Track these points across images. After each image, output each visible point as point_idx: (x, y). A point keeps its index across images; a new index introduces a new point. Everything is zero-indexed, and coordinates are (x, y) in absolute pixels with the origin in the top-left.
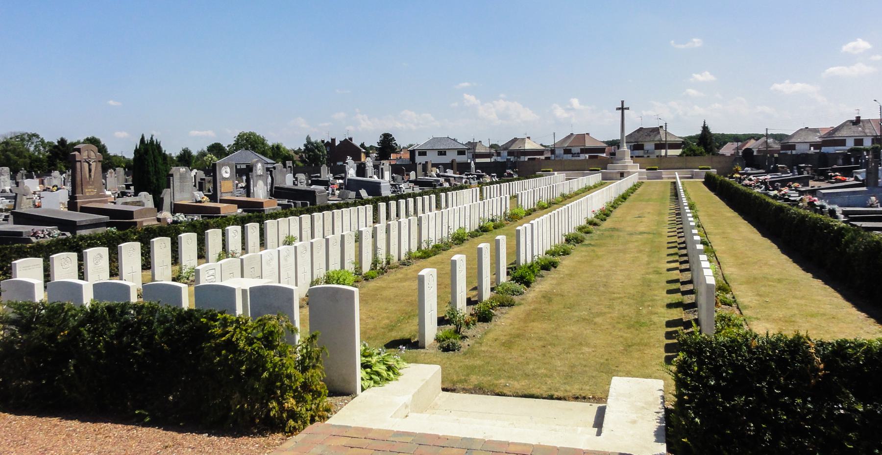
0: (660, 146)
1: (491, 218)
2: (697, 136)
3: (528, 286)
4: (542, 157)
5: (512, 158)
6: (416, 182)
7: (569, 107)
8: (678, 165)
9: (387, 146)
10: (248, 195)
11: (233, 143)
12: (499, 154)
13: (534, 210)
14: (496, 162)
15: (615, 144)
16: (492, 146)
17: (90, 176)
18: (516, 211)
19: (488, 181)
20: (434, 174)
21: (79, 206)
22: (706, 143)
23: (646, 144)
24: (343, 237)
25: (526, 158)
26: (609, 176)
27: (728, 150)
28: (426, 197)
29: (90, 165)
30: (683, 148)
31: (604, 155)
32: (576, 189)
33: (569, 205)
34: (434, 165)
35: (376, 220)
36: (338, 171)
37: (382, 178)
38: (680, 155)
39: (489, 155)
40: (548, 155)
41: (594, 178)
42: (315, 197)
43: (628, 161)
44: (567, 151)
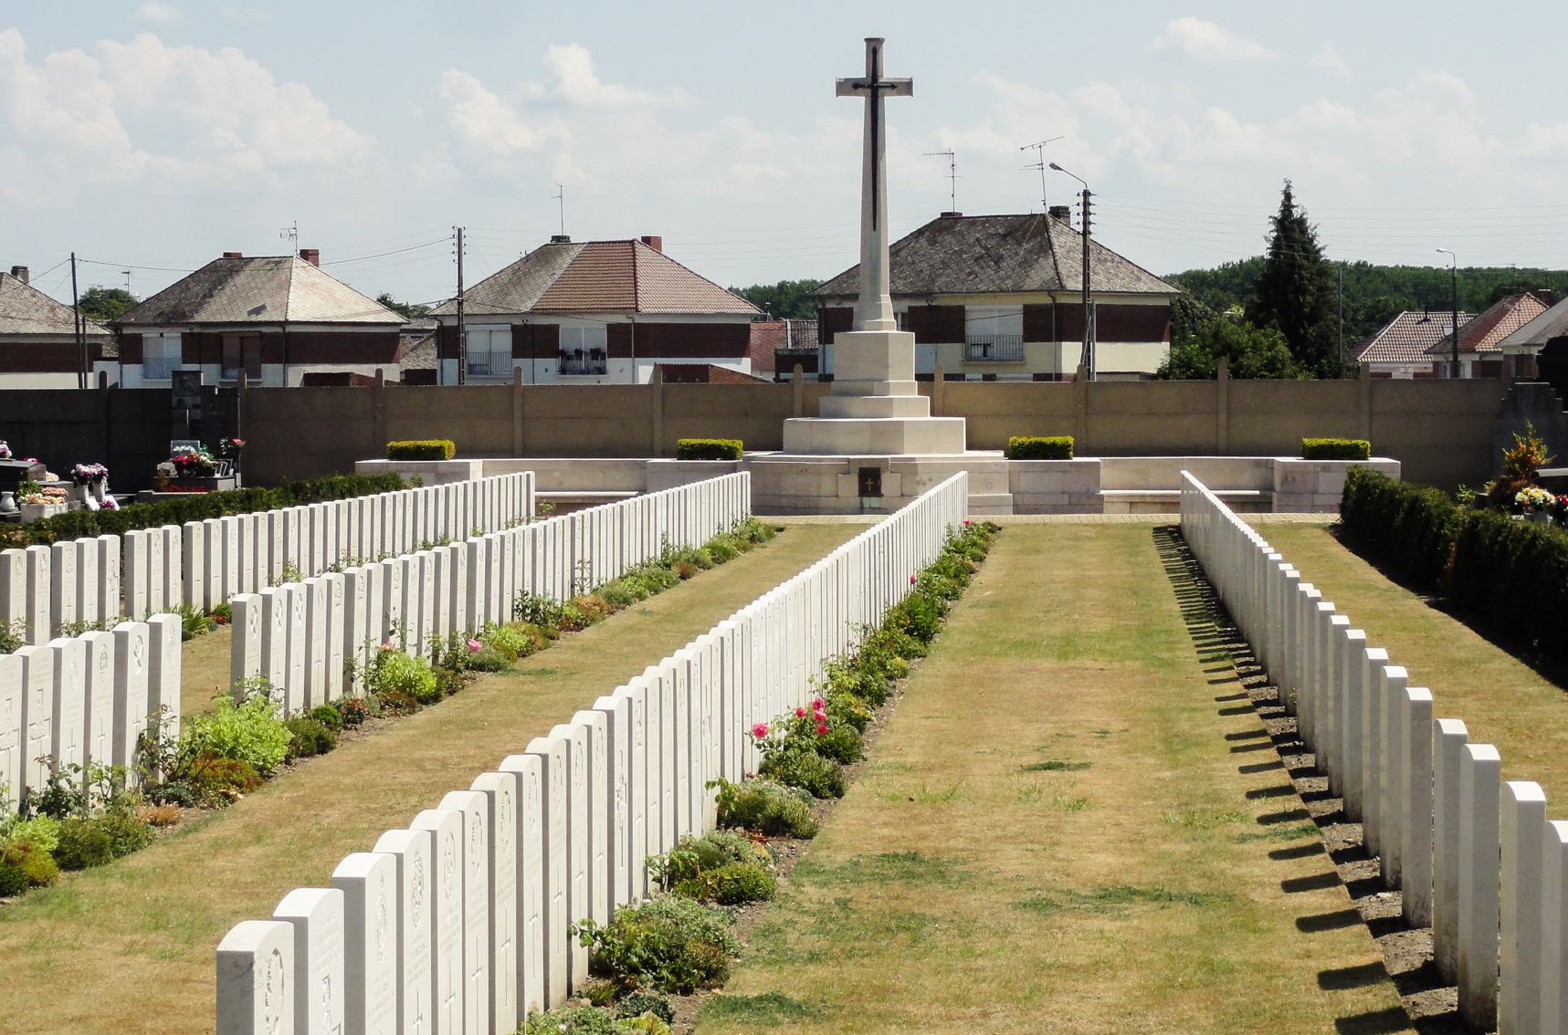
0: (1053, 321)
1: (39, 783)
4: (392, 373)
5: (209, 375)
7: (536, 90)
8: (1193, 427)
12: (130, 350)
13: (352, 715)
14: (110, 396)
15: (829, 308)
16: (91, 305)
18: (230, 724)
19: (54, 507)
22: (1289, 309)
23: (984, 297)
25: (295, 376)
26: (792, 485)
27: (1402, 348)
30: (1176, 338)
31: (743, 366)
32: (605, 571)
33: (613, 701)
38: (1163, 375)
40: (426, 358)
41: (708, 504)
43: (906, 402)
44: (534, 339)
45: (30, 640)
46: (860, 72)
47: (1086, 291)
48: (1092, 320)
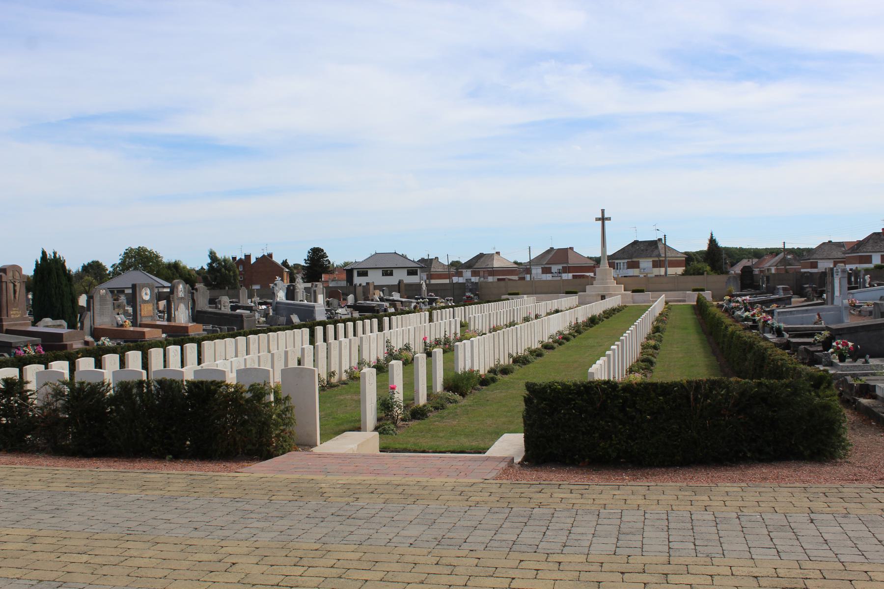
3: (464, 396)
6: (355, 307)
10: (169, 320)
11: (118, 261)
15: (598, 261)
17: (15, 297)
20: (377, 297)
21: (5, 328)
24: (286, 353)
28: (367, 321)
29: (15, 286)
34: (377, 287)
35: (312, 341)
36: (268, 294)
37: (315, 301)
38: (683, 275)
39: (449, 276)
42: (242, 321)
46: (600, 216)
47: (665, 257)
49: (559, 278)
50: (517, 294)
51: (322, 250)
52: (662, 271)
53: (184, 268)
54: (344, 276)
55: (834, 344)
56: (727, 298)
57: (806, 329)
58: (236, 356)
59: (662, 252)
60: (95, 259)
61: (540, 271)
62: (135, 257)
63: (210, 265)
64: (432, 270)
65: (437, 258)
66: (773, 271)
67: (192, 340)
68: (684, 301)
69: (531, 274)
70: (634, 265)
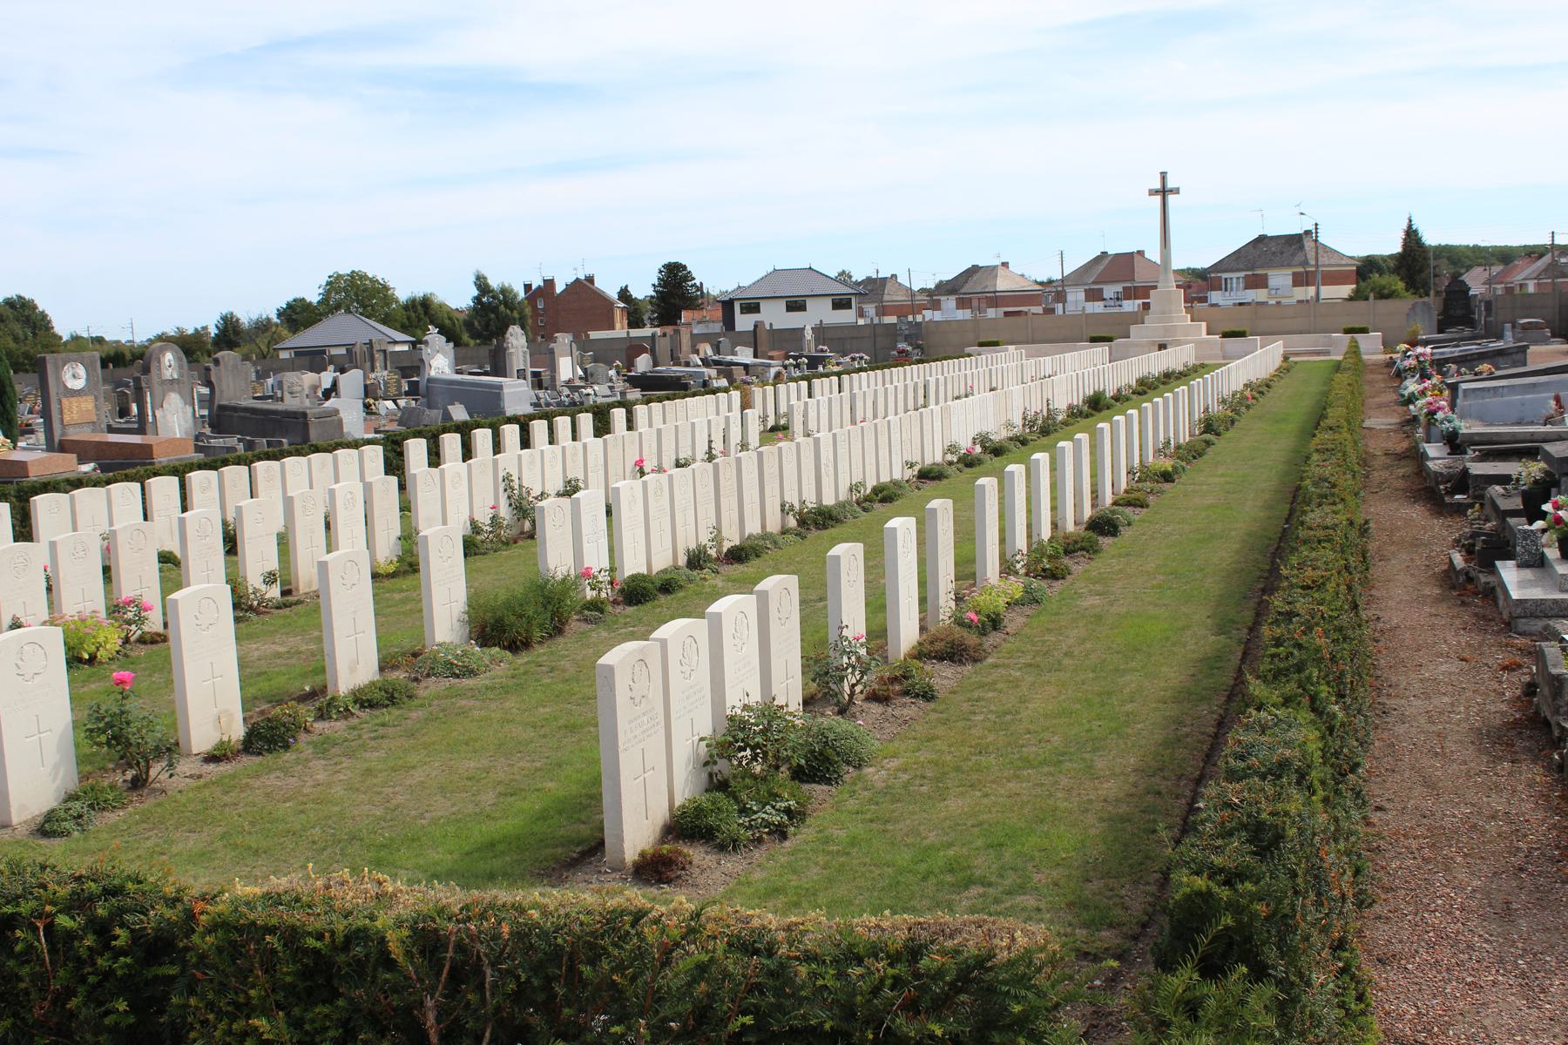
2: (1391, 257)
9: (676, 290)
38: (1351, 299)
42: (306, 425)
45: (587, 488)
46: (1158, 186)
47: (1317, 265)
48: (1319, 277)
49: (1116, 310)
50: (996, 344)
51: (684, 267)
52: (1311, 291)
53: (441, 306)
54: (719, 314)
55: (1547, 507)
56: (1404, 346)
57: (1515, 438)
58: (551, 443)
59: (1311, 255)
60: (299, 296)
61: (1082, 296)
62: (345, 289)
63: (477, 299)
64: (886, 298)
65: (894, 276)
66: (1531, 289)
67: (510, 420)
68: (1327, 353)
69: (1064, 302)
70: (1258, 282)
